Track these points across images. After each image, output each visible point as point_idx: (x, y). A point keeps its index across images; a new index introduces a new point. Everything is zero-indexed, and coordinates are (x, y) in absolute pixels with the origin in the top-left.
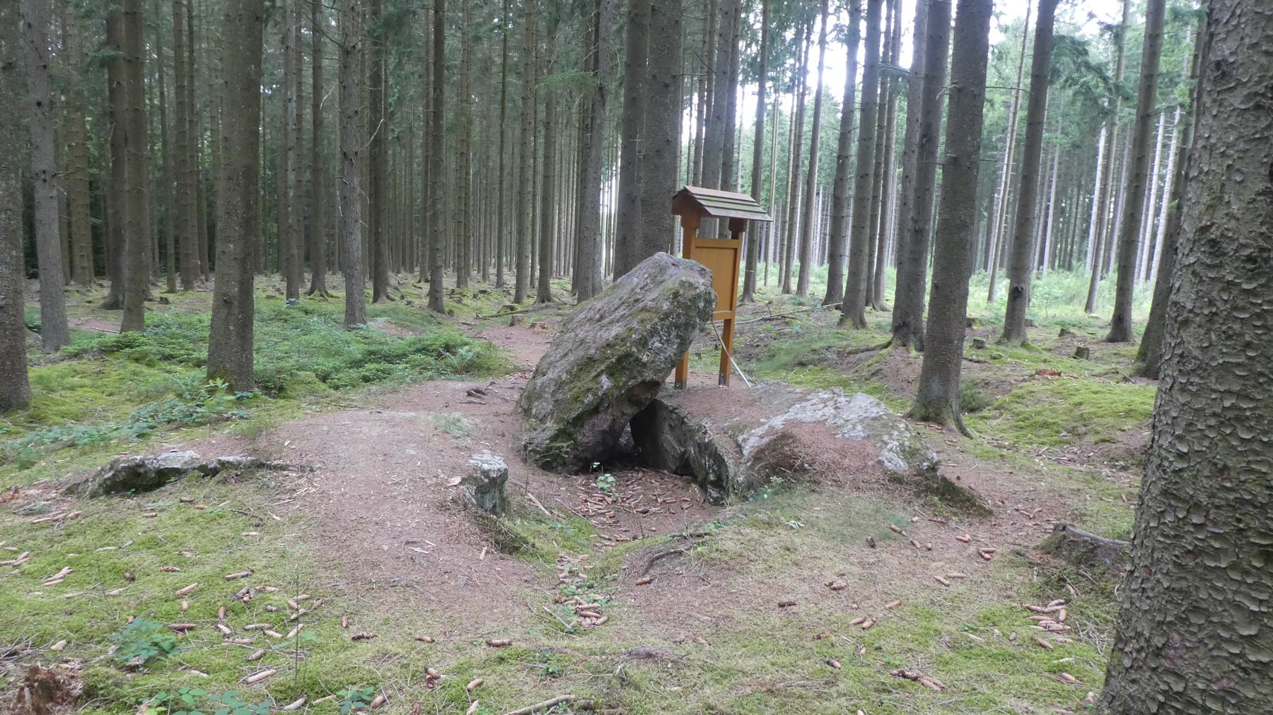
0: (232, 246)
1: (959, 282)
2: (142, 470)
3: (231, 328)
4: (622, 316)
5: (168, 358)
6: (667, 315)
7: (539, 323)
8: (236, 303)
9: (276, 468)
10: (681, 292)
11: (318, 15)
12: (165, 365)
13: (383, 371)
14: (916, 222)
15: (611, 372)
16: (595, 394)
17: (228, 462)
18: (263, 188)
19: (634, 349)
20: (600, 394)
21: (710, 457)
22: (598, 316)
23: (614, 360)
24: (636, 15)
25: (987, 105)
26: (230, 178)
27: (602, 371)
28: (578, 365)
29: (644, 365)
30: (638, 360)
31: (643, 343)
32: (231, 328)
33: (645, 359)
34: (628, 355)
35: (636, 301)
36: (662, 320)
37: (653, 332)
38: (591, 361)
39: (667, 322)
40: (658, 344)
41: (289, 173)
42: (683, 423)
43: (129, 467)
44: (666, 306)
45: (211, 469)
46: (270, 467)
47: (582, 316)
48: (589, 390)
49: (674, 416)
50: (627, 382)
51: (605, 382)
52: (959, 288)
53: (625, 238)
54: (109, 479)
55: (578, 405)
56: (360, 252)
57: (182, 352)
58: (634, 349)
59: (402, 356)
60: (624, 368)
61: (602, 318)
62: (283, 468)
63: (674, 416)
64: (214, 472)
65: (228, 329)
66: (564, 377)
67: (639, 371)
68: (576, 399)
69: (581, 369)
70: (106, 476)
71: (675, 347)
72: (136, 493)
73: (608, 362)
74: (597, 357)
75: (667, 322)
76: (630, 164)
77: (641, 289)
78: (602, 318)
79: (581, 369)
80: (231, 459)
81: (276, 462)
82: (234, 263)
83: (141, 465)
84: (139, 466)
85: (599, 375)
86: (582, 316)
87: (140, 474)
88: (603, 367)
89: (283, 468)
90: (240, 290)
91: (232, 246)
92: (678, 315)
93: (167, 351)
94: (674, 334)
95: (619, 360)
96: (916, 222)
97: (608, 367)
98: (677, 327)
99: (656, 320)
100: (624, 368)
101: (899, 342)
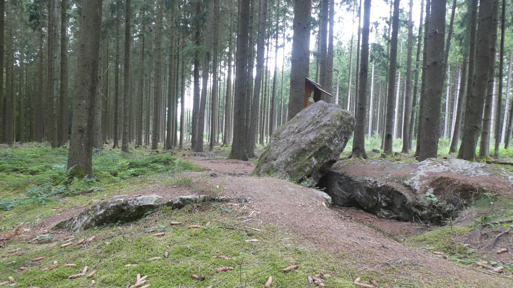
0: (84, 101)
1: (437, 117)
2: (125, 208)
3: (83, 145)
4: (312, 130)
5: (15, 170)
6: (340, 127)
7: (187, 154)
8: (86, 131)
9: (222, 201)
10: (344, 116)
11: (64, 24)
12: (15, 173)
13: (142, 171)
14: (361, 105)
15: (316, 156)
16: (310, 167)
17: (187, 199)
18: (19, 109)
19: (327, 144)
20: (313, 167)
21: (382, 194)
22: (297, 130)
23: (317, 149)
24: (245, 14)
25: (334, 73)
26: (85, 66)
27: (312, 155)
28: (297, 153)
29: (331, 152)
30: (329, 149)
31: (330, 141)
32: (83, 145)
33: (332, 149)
34: (325, 147)
35: (317, 122)
36: (338, 129)
37: (335, 136)
38: (303, 152)
39: (340, 131)
40: (337, 141)
41: (54, 90)
42: (351, 180)
43: (117, 206)
44: (338, 123)
45: (176, 204)
46: (219, 201)
47: (285, 131)
48: (307, 165)
49: (343, 177)
50: (323, 161)
51: (314, 161)
52: (437, 119)
53: (240, 112)
54: (101, 215)
55: (301, 173)
56: (101, 123)
57: (23, 167)
58: (327, 144)
59: (146, 165)
60: (322, 153)
61: (299, 131)
62: (227, 201)
63: (343, 177)
64: (179, 206)
65: (81, 145)
66: (289, 159)
67: (329, 155)
68: (300, 170)
69: (299, 155)
70: (99, 213)
71: (343, 143)
72: (122, 223)
73: (314, 151)
74: (306, 149)
75: (340, 131)
76: (242, 79)
77: (318, 116)
78: (299, 131)
79: (299, 155)
80: (190, 197)
81: (222, 197)
82: (85, 110)
83: (125, 204)
84: (123, 205)
85: (310, 157)
86: (285, 131)
87: (123, 211)
88: (312, 153)
89: (227, 201)
90: (88, 125)
91: (84, 101)
92: (344, 127)
93: (15, 167)
94: (343, 136)
95: (320, 150)
96: (361, 105)
97: (315, 154)
98: (344, 133)
99: (335, 130)
100: (322, 153)
101: (356, 155)
